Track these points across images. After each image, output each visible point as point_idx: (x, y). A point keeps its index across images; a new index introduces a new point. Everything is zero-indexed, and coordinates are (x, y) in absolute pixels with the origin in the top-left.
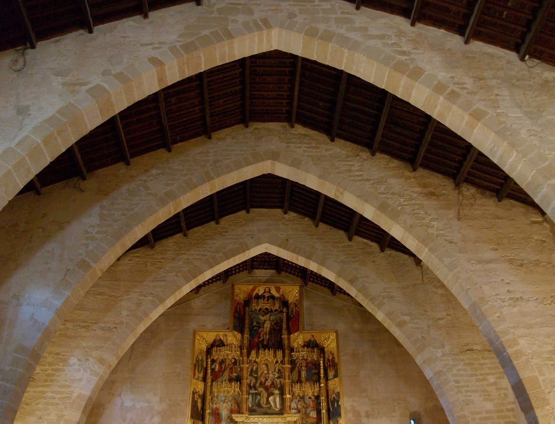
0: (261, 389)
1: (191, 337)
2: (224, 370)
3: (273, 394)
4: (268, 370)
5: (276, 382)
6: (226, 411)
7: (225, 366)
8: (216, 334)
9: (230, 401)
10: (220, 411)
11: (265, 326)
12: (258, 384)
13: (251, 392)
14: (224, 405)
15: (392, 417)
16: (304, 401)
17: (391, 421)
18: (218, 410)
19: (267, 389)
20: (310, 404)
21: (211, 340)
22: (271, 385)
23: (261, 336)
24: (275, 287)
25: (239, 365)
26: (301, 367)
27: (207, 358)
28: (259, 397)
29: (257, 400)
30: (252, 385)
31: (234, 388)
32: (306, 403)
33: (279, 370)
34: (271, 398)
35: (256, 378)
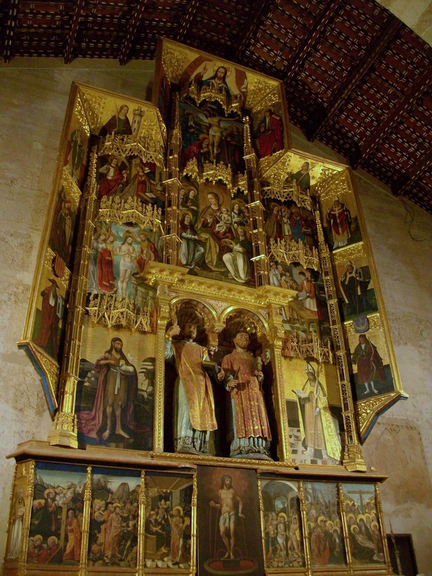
0: (204, 236)
1: (66, 99)
2: (127, 183)
3: (230, 250)
4: (220, 206)
5: (236, 230)
6: (128, 260)
7: (129, 175)
8: (120, 103)
9: (138, 243)
10: (115, 259)
11: (211, 132)
12: (199, 225)
13: (184, 234)
14: (125, 248)
15: (420, 346)
16: (291, 275)
17: (420, 353)
18: (110, 255)
19: (217, 237)
20: (302, 284)
21: (104, 118)
22: (225, 233)
23: (204, 145)
24: (237, 70)
25: (161, 180)
26: (282, 217)
27: (90, 151)
28: (202, 250)
29: (197, 254)
30: (186, 223)
31: (151, 218)
32: (295, 282)
33: (240, 212)
34: (227, 257)
35: (195, 213)
